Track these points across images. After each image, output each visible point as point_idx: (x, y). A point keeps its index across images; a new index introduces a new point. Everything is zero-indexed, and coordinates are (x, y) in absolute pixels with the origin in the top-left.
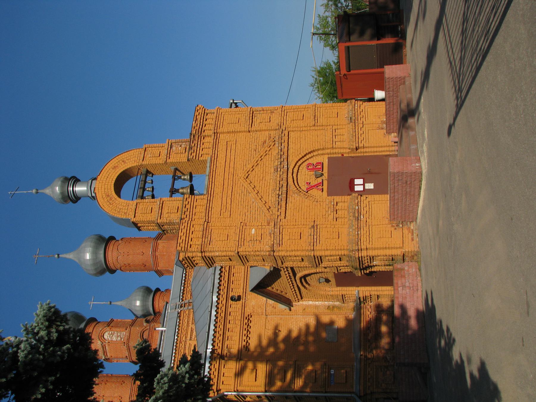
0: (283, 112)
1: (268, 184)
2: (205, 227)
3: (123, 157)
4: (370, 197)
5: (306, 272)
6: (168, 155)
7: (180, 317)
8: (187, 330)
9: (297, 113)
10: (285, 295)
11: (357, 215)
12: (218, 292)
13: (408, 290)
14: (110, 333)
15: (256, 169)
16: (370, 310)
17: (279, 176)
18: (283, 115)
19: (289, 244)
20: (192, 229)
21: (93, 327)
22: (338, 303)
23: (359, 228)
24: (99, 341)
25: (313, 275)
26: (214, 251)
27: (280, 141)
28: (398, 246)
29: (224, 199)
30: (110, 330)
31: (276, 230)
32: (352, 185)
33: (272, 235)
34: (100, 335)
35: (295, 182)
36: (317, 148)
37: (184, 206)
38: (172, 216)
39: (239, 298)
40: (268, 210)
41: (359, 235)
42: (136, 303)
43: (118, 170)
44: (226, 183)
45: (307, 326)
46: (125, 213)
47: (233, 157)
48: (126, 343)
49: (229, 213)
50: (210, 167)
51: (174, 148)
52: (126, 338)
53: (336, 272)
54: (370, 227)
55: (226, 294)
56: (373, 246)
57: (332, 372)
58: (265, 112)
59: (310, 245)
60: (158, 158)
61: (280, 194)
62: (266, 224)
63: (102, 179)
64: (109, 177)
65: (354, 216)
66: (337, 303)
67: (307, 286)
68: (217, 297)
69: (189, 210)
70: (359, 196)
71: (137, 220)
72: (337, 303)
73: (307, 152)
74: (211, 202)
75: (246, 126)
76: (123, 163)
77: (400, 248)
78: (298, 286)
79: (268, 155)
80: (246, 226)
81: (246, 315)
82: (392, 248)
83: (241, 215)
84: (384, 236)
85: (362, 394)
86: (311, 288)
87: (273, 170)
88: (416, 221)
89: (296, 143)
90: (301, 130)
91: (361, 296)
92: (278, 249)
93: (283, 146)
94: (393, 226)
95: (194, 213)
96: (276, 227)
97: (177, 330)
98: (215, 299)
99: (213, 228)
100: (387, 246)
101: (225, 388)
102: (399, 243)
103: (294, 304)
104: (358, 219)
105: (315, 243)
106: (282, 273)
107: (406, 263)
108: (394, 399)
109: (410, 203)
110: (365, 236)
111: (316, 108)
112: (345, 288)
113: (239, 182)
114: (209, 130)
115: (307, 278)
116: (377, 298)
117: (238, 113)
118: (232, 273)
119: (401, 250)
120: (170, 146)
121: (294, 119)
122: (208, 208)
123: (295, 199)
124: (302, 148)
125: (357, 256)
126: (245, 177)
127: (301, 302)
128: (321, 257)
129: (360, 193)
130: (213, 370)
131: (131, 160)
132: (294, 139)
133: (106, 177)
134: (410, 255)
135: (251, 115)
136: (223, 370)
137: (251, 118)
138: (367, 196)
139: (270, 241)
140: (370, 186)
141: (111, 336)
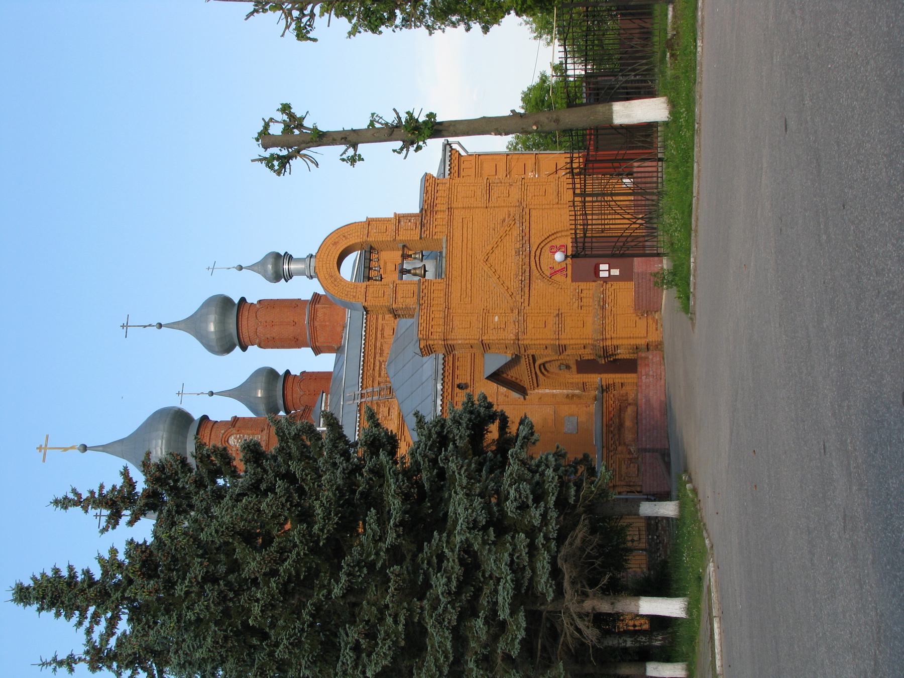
0: (523, 186)
1: (510, 268)
2: (446, 314)
3: (344, 232)
4: (616, 285)
5: (548, 359)
6: (397, 232)
7: (360, 410)
9: (539, 187)
10: (519, 383)
11: (602, 304)
12: (442, 379)
13: (651, 379)
14: (238, 436)
15: (496, 251)
16: (613, 399)
17: (521, 260)
18: (523, 190)
19: (533, 331)
20: (432, 316)
21: (210, 429)
23: (604, 318)
25: (553, 362)
26: (457, 339)
27: (521, 221)
28: (642, 336)
29: (464, 283)
30: (237, 432)
31: (520, 318)
32: (597, 271)
34: (223, 439)
35: (538, 266)
36: (560, 230)
37: (421, 290)
38: (408, 300)
41: (604, 325)
44: (464, 267)
46: (354, 297)
49: (470, 299)
50: (446, 248)
51: (402, 223)
53: (579, 359)
54: (615, 315)
55: (451, 381)
56: (618, 336)
58: (503, 184)
59: (555, 334)
60: (385, 234)
61: (523, 279)
62: (509, 311)
63: (322, 257)
64: (330, 254)
65: (599, 305)
66: (577, 392)
67: (546, 373)
68: (442, 384)
69: (427, 295)
70: (605, 284)
71: (369, 304)
72: (577, 392)
73: (551, 234)
74: (450, 287)
75: (483, 201)
76: (344, 239)
77: (644, 337)
78: (536, 373)
79: (508, 236)
80: (489, 313)
82: (636, 338)
83: (483, 301)
84: (629, 325)
86: (549, 375)
87: (514, 253)
88: (661, 311)
90: (544, 207)
91: (604, 384)
92: (522, 338)
93: (524, 226)
94: (637, 316)
95: (432, 298)
96: (520, 314)
97: (358, 428)
98: (439, 387)
99: (454, 314)
100: (632, 336)
102: (643, 332)
103: (528, 392)
104: (603, 308)
105: (560, 332)
106: (523, 360)
107: (650, 352)
109: (654, 296)
110: (610, 325)
111: (560, 183)
113: (478, 266)
114: (441, 206)
115: (546, 365)
116: (621, 387)
117: (472, 185)
118: (457, 358)
119: (645, 339)
120: (397, 221)
121: (536, 194)
122: (447, 293)
123: (539, 285)
125: (601, 345)
126: (485, 260)
127: (536, 391)
128: (565, 346)
129: (605, 280)
132: (536, 217)
134: (654, 344)
135: (488, 188)
137: (488, 191)
138: (612, 283)
139: (514, 330)
140: (615, 272)
141: (239, 441)
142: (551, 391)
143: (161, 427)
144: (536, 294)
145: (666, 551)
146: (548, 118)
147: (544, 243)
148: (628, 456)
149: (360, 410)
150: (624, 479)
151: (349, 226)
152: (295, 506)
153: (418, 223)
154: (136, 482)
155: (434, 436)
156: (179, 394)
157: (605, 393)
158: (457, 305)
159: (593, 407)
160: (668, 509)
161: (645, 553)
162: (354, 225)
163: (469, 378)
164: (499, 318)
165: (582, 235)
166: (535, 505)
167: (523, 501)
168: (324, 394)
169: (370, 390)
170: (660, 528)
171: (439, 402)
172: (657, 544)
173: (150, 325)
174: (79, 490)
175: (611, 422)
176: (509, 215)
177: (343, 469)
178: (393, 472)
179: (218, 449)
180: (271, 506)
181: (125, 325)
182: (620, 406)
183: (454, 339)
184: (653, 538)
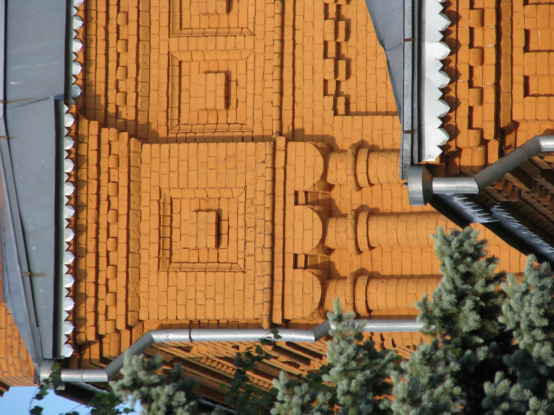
40: (274, 40)
101: (542, 115)
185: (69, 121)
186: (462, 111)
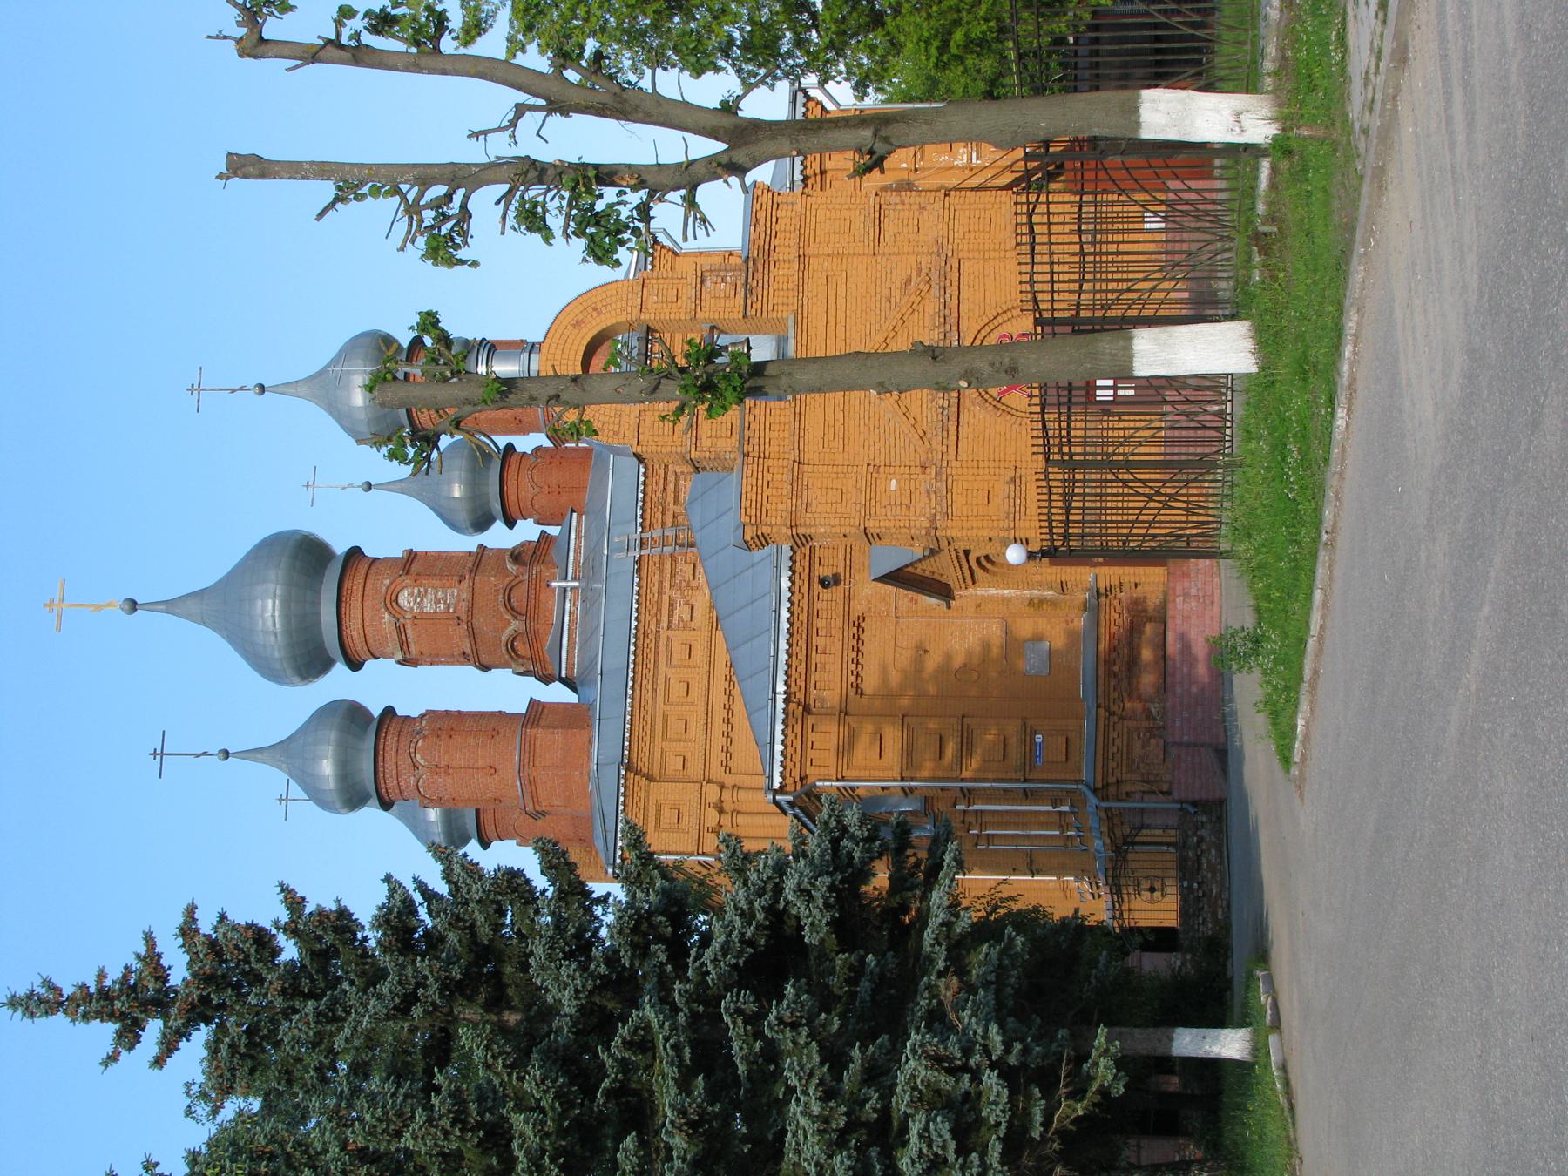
2: (795, 474)
7: (639, 571)
8: (659, 603)
9: (977, 212)
10: (938, 578)
18: (946, 219)
20: (768, 477)
21: (363, 576)
22: (1051, 593)
24: (386, 615)
33: (933, 496)
39: (836, 580)
42: (450, 491)
43: (584, 330)
45: (986, 646)
46: (616, 433)
47: (841, 315)
48: (464, 617)
50: (796, 337)
51: (708, 284)
52: (464, 605)
57: (1039, 738)
58: (907, 207)
59: (1007, 517)
61: (946, 405)
63: (552, 351)
64: (568, 346)
71: (644, 448)
72: (1049, 593)
76: (595, 314)
78: (970, 567)
81: (854, 617)
85: (1099, 785)
86: (995, 569)
89: (977, 287)
93: (948, 296)
97: (635, 606)
98: (785, 583)
103: (956, 593)
108: (1162, 793)
112: (1068, 569)
114: (785, 250)
124: (988, 301)
127: (971, 590)
130: (791, 736)
131: (614, 306)
133: (561, 347)
135: (877, 214)
136: (811, 737)
137: (877, 221)
142: (1000, 592)
143: (272, 575)
144: (971, 436)
145: (1214, 914)
146: (992, 365)
147: (987, 329)
148: (1145, 724)
149: (639, 571)
150: (1138, 768)
151: (604, 289)
152: (472, 1130)
153: (739, 283)
154: (170, 968)
155: (760, 916)
156: (307, 486)
157: (1103, 599)
158: (817, 455)
159: (1080, 622)
160: (1230, 1044)
161: (1172, 850)
162: (614, 286)
163: (842, 564)
164: (898, 482)
165: (1062, 531)
166: (960, 1160)
167: (936, 1155)
168: (575, 515)
169: (657, 533)
170: (1205, 866)
171: (785, 614)
172: (1198, 899)
173: (242, 389)
174: (58, 982)
175: (1114, 655)
176: (919, 270)
177: (577, 991)
178: (672, 1047)
179: (328, 918)
180: (423, 1138)
181: (196, 386)
182: (1132, 622)
183: (810, 526)
184: (1190, 887)
185: (623, 772)
186: (788, 770)
